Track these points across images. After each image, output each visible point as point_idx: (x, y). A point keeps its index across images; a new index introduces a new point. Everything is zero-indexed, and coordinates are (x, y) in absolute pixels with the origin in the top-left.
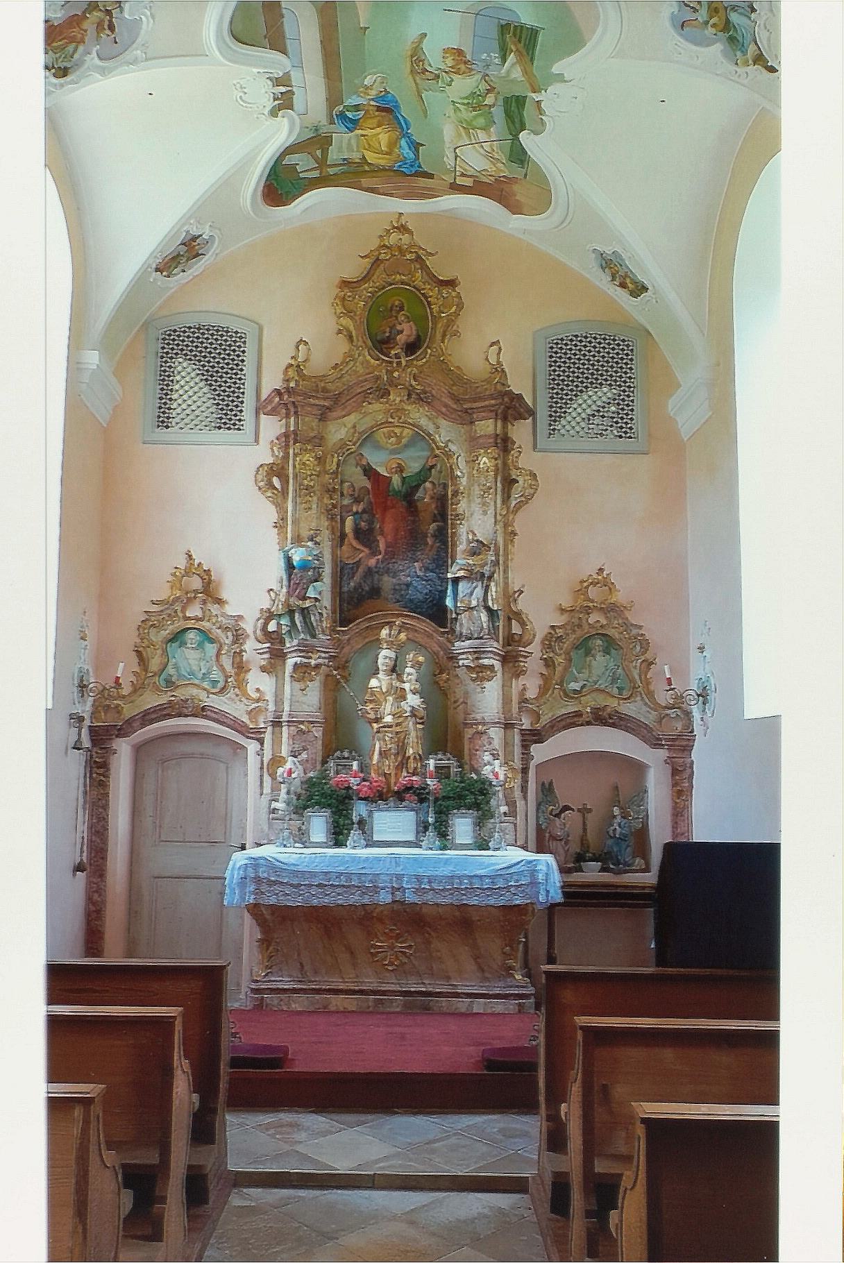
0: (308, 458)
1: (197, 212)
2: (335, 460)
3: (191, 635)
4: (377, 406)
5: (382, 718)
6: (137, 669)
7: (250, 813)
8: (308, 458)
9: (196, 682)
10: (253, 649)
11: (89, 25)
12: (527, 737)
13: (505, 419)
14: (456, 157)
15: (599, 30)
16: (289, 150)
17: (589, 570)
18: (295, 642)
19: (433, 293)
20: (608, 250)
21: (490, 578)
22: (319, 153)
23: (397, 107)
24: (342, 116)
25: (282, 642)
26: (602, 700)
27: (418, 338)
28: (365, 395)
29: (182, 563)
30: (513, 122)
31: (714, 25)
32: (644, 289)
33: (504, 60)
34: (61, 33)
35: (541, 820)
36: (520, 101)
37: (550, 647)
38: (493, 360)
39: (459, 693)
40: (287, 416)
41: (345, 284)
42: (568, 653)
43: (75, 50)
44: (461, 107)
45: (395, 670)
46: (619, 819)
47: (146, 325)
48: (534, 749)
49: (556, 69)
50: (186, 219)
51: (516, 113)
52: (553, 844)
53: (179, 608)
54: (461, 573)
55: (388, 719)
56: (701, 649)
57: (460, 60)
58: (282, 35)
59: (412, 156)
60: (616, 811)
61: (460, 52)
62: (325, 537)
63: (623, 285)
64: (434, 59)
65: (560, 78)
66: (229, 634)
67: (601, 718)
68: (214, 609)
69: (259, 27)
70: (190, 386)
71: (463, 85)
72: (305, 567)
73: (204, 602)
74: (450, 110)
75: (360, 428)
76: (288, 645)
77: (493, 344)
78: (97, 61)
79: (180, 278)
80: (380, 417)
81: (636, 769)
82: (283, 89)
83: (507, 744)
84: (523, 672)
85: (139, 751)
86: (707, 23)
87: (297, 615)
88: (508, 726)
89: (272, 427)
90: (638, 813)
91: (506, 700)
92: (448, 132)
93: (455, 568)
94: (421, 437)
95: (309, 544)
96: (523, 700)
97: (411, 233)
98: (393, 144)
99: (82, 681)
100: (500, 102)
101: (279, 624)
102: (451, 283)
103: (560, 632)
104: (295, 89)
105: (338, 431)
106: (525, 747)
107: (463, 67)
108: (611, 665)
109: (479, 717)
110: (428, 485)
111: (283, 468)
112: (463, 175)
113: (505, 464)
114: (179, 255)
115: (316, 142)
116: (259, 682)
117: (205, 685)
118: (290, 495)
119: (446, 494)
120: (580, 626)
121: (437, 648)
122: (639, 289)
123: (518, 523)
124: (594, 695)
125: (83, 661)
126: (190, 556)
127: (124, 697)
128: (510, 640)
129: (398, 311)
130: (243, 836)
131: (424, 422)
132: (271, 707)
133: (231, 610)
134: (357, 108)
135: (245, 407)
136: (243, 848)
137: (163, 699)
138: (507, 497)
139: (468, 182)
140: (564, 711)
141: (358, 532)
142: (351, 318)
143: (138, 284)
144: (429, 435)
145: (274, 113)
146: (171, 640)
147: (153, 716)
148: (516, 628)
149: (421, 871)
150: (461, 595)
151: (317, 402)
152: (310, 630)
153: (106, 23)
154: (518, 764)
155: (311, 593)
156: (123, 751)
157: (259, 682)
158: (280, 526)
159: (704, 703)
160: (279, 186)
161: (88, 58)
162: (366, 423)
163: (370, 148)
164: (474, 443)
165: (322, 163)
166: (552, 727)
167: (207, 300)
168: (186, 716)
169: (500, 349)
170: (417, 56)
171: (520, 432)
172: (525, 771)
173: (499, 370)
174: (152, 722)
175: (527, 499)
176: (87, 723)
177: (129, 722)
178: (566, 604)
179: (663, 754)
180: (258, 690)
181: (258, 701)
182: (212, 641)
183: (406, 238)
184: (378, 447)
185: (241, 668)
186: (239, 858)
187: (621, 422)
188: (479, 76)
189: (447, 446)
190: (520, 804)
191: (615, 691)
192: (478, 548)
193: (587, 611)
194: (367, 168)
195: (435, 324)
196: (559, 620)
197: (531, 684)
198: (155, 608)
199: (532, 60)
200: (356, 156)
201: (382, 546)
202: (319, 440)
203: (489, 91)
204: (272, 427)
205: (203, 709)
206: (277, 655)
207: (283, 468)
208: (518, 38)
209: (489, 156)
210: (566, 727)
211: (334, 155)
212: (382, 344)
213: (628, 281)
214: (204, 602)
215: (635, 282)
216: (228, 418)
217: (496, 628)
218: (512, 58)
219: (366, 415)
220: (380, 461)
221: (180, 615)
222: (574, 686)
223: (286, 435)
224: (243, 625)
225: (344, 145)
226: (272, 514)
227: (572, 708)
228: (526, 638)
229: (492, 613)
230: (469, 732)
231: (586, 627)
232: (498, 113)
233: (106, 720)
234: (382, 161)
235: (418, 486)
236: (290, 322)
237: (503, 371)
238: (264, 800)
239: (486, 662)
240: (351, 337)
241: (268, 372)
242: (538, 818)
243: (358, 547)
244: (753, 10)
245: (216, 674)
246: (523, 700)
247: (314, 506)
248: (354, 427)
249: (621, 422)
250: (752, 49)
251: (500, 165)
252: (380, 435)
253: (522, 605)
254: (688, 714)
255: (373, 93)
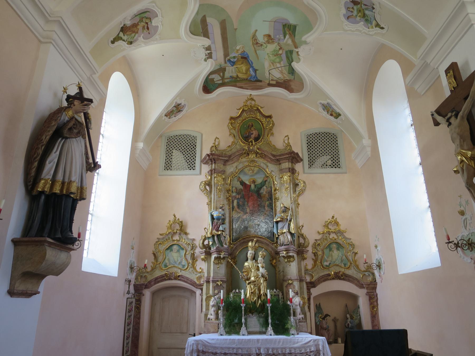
0: (220, 179)
1: (179, 95)
2: (229, 179)
3: (175, 247)
4: (244, 160)
5: (250, 278)
6: (153, 261)
7: (197, 320)
8: (220, 179)
9: (176, 265)
10: (198, 251)
11: (140, 27)
12: (309, 285)
13: (292, 163)
14: (269, 73)
15: (318, 23)
16: (211, 73)
17: (328, 217)
18: (215, 248)
19: (264, 120)
20: (325, 102)
21: (290, 221)
22: (221, 74)
23: (248, 57)
24: (229, 60)
25: (210, 249)
26: (337, 269)
27: (259, 135)
28: (241, 155)
29: (172, 218)
30: (289, 60)
31: (360, 16)
32: (340, 115)
33: (285, 37)
34: (130, 29)
35: (317, 320)
36: (291, 52)
37: (315, 248)
38: (286, 142)
39: (281, 268)
40: (212, 164)
41: (232, 118)
42: (323, 250)
43: (135, 36)
44: (270, 55)
45: (255, 258)
46: (349, 320)
47: (161, 136)
48: (312, 290)
49: (304, 38)
50: (175, 98)
51: (290, 56)
52: (325, 332)
53: (170, 237)
54: (279, 219)
55: (253, 279)
56: (376, 247)
57: (270, 39)
58: (207, 31)
59: (254, 74)
60: (348, 316)
61: (269, 36)
62: (227, 207)
63: (331, 115)
64: (261, 39)
65: (305, 43)
66: (190, 246)
67: (338, 276)
68: (184, 236)
69: (200, 28)
70: (177, 157)
71: (271, 47)
72: (218, 219)
73: (180, 234)
74: (267, 57)
75: (239, 168)
76: (212, 249)
77: (286, 136)
78: (143, 40)
79: (174, 119)
80: (246, 164)
81: (354, 298)
82: (209, 52)
83: (301, 288)
84: (305, 259)
85: (154, 294)
86: (357, 16)
87: (215, 237)
88: (301, 280)
89: (206, 168)
90: (357, 317)
91: (300, 270)
92: (267, 64)
93: (276, 218)
94: (261, 170)
95: (220, 210)
96: (306, 270)
97: (255, 101)
98: (247, 70)
99: (131, 266)
100: (284, 53)
101: (209, 242)
102: (270, 117)
103: (319, 242)
104: (212, 52)
105: (230, 169)
106: (309, 289)
107: (270, 41)
108: (340, 254)
109: (289, 277)
110: (265, 187)
111: (210, 182)
112: (272, 80)
113: (293, 178)
114: (173, 111)
115: (220, 70)
116: (201, 265)
117: (180, 266)
118: (213, 193)
119: (272, 191)
120: (326, 239)
121: (271, 250)
122: (338, 115)
123: (300, 201)
124: (335, 267)
125: (132, 258)
126: (175, 216)
127: (148, 272)
128: (300, 245)
129: (251, 128)
130: (194, 330)
131: (262, 165)
132: (206, 275)
133: (190, 237)
134: (234, 57)
135: (197, 159)
136: (194, 335)
137: (163, 273)
138: (295, 191)
139: (274, 82)
140: (323, 274)
141: (238, 206)
142: (235, 130)
143: (158, 121)
144: (264, 169)
145: (205, 60)
146: (167, 249)
147: (159, 280)
148: (302, 241)
149: (268, 346)
150: (279, 228)
151: (222, 158)
152: (221, 243)
153: (146, 28)
154: (306, 296)
155: (221, 228)
156: (147, 294)
157: (201, 265)
158: (209, 204)
159: (380, 269)
160: (208, 88)
161: (139, 38)
162: (240, 166)
163: (239, 72)
164: (281, 171)
165: (223, 78)
166: (319, 281)
167: (182, 126)
168: (172, 279)
169: (289, 138)
170: (254, 37)
171: (298, 167)
172: (309, 299)
173: (289, 145)
174: (158, 282)
175: (303, 191)
176: (133, 283)
177: (150, 282)
178: (321, 230)
179: (365, 291)
180: (200, 268)
181: (200, 273)
182: (183, 249)
183: (253, 102)
184: (245, 174)
185: (194, 258)
186: (191, 340)
187: (335, 163)
188: (276, 44)
189: (271, 173)
190: (308, 314)
191: (343, 265)
192: (286, 210)
193: (329, 233)
194: (238, 79)
195: (264, 131)
196: (319, 237)
197: (309, 263)
198: (161, 237)
199: (295, 36)
200: (235, 75)
201: (248, 210)
202: (223, 172)
203: (280, 49)
204: (206, 168)
205: (179, 276)
206: (208, 254)
207: (210, 182)
208: (289, 29)
209: (281, 72)
210: (324, 281)
211: (227, 75)
212: (246, 138)
213: (333, 113)
214: (180, 234)
215: (336, 113)
216: (192, 166)
217: (294, 241)
218: (287, 36)
219: (240, 163)
220: (246, 180)
221: (171, 239)
222: (326, 264)
223: (211, 171)
224: (195, 242)
225: (230, 71)
226: (206, 200)
227: (326, 272)
228: (306, 244)
229: (292, 234)
230: (285, 284)
231: (329, 240)
232: (284, 56)
233: (142, 281)
234: (245, 77)
235: (261, 188)
236: (211, 129)
237: (290, 145)
238: (203, 315)
239: (291, 254)
240: (234, 136)
241: (204, 149)
242: (315, 320)
243: (239, 211)
244: (373, 8)
245: (184, 262)
246: (306, 270)
247: (222, 196)
248: (236, 167)
249: (335, 163)
250: (374, 23)
251: (285, 75)
252: (246, 170)
253: (304, 231)
254: (373, 274)
255: (240, 52)
